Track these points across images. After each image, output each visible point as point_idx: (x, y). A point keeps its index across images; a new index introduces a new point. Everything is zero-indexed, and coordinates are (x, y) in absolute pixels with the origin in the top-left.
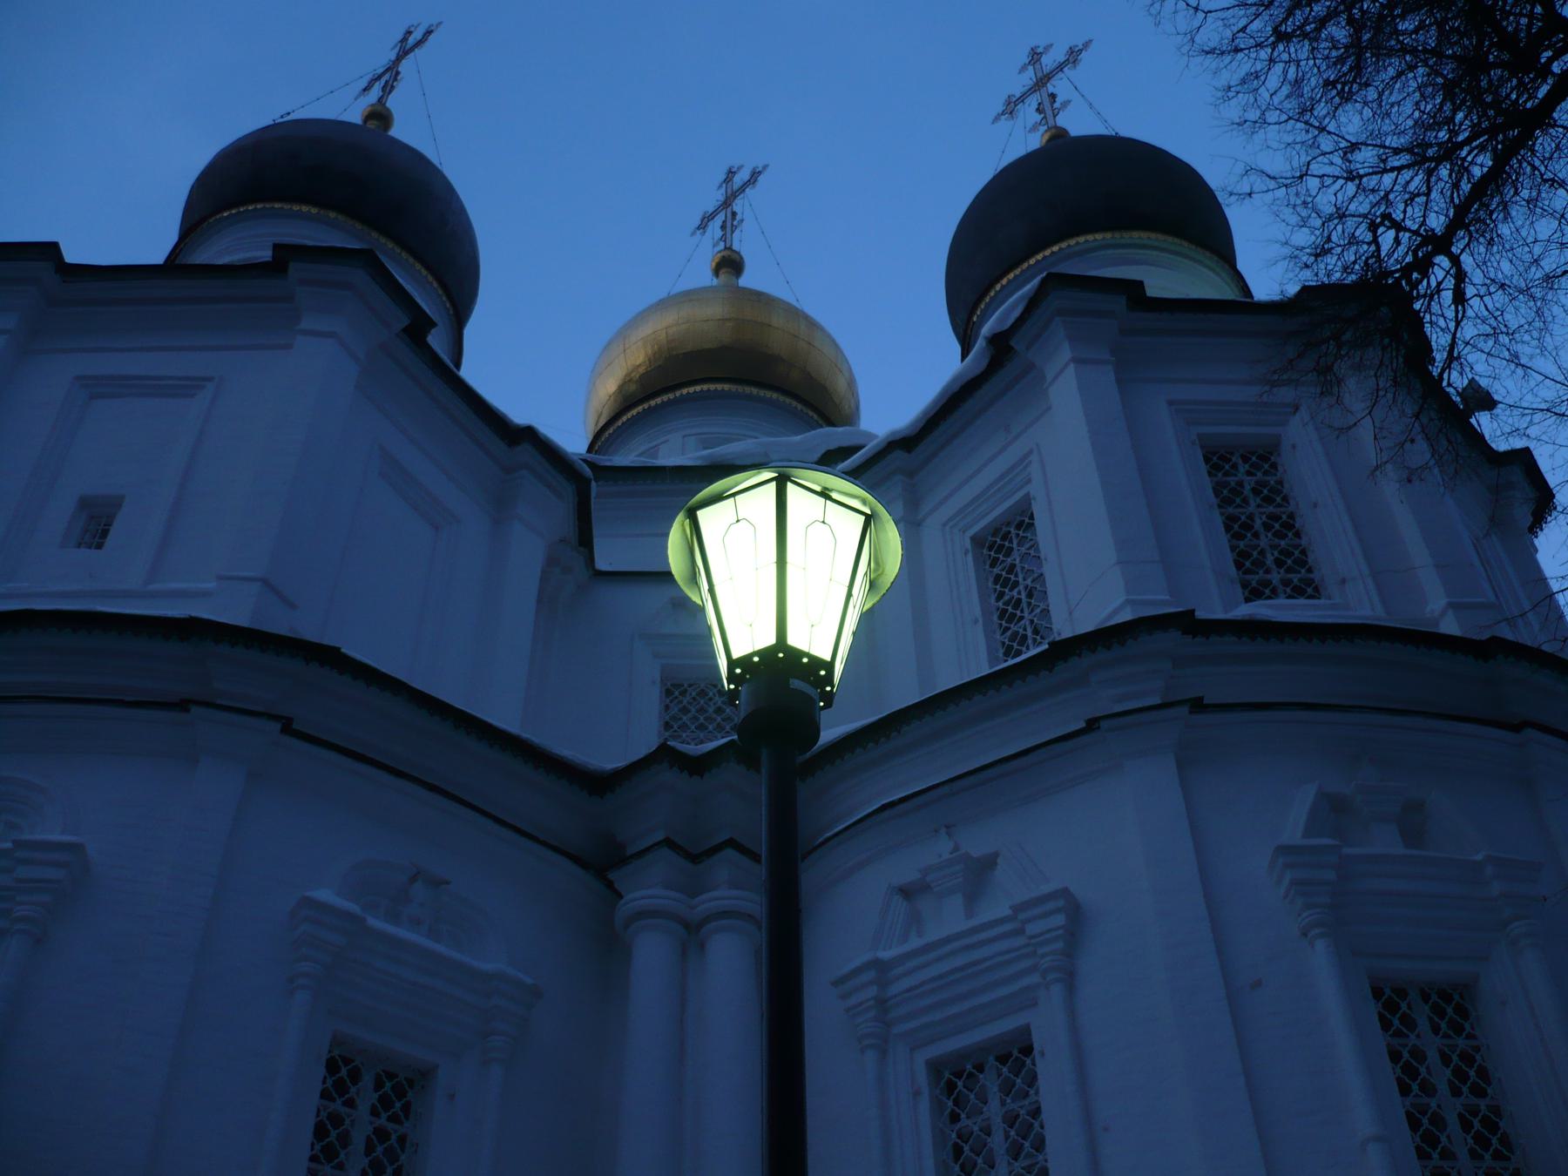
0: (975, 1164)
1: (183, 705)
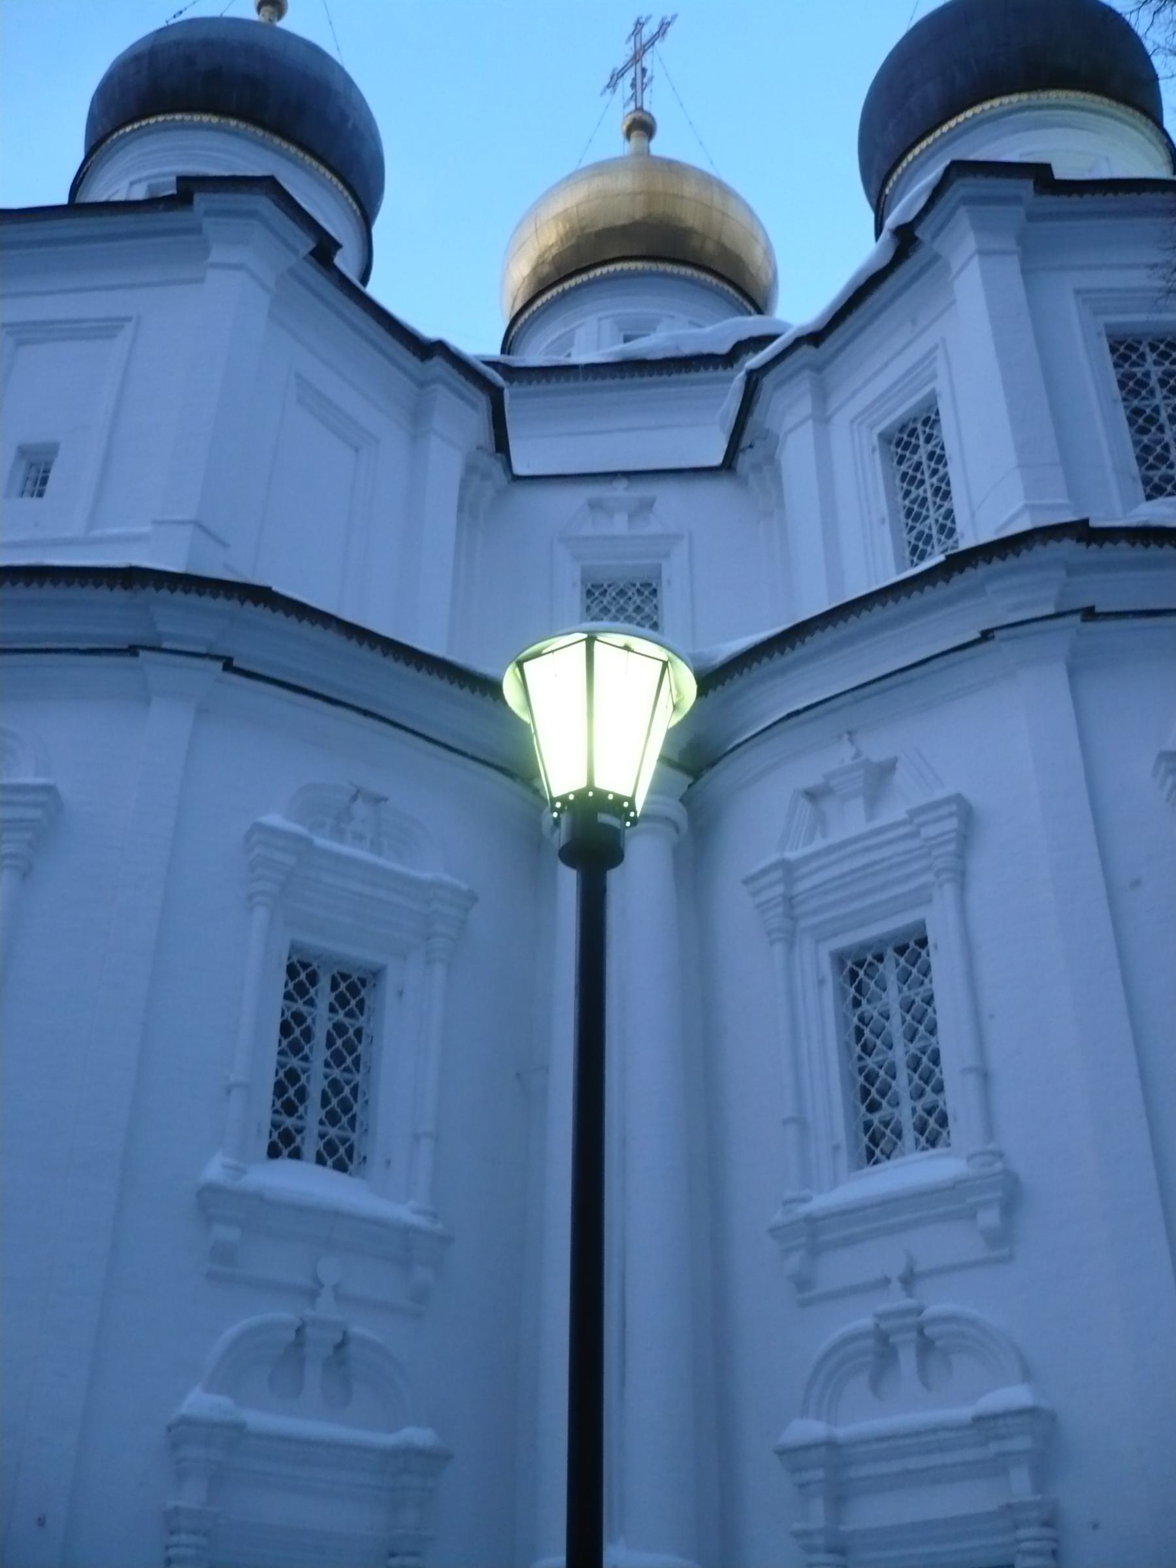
0: (875, 1046)
1: (132, 650)
